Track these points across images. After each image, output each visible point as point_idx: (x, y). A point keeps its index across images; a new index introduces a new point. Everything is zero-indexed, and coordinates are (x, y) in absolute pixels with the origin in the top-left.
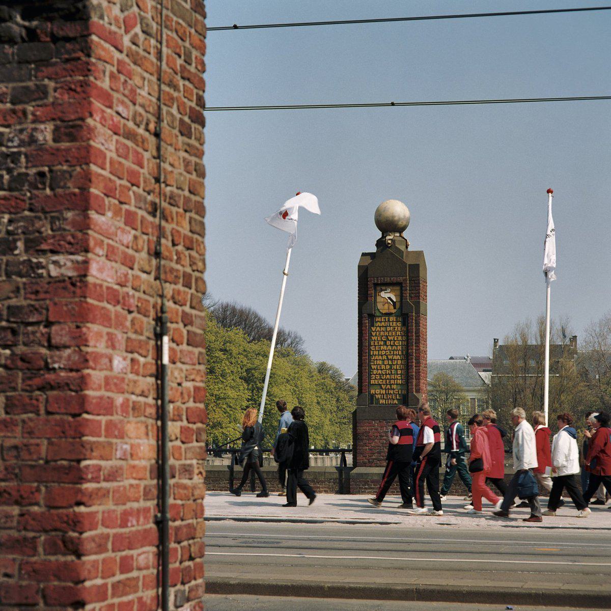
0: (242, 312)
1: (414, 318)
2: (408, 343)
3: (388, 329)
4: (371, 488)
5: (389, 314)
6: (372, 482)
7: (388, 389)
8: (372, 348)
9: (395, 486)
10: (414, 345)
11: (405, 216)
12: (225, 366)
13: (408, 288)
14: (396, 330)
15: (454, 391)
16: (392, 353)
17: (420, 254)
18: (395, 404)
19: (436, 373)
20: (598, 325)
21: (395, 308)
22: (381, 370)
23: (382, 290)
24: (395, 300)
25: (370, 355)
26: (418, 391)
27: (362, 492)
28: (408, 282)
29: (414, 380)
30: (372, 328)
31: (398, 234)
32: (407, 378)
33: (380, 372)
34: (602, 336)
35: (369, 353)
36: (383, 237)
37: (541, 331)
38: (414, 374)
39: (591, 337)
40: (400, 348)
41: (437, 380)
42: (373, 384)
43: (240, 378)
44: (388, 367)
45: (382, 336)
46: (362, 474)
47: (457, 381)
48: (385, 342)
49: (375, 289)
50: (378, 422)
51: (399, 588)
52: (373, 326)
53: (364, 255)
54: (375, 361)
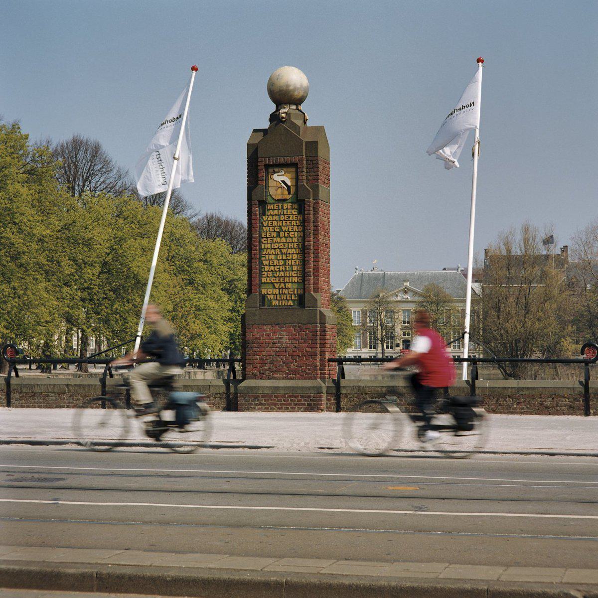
0: (227, 224)
1: (312, 205)
2: (304, 234)
3: (282, 218)
4: (262, 404)
5: (283, 201)
6: (263, 396)
7: (282, 288)
8: (263, 240)
9: (290, 402)
10: (312, 236)
11: (301, 86)
12: (205, 277)
13: (305, 170)
14: (291, 219)
15: (445, 302)
16: (286, 246)
17: (320, 130)
18: (290, 305)
19: (427, 283)
20: (584, 233)
21: (289, 193)
22: (274, 266)
23: (274, 172)
24: (289, 184)
25: (260, 249)
26: (316, 290)
27: (252, 408)
28: (305, 162)
29: (312, 278)
30: (264, 217)
31: (294, 107)
32: (304, 275)
33: (272, 268)
34: (587, 243)
35: (260, 246)
36: (278, 110)
37: (525, 239)
38: (312, 270)
39: (577, 245)
40: (295, 240)
41: (428, 291)
42: (265, 283)
43: (222, 290)
44: (282, 262)
45: (275, 226)
46: (251, 388)
47: (447, 292)
48: (279, 233)
49: (267, 170)
50: (270, 326)
51: (71, 571)
52: (264, 214)
53: (255, 131)
54: (267, 256)
